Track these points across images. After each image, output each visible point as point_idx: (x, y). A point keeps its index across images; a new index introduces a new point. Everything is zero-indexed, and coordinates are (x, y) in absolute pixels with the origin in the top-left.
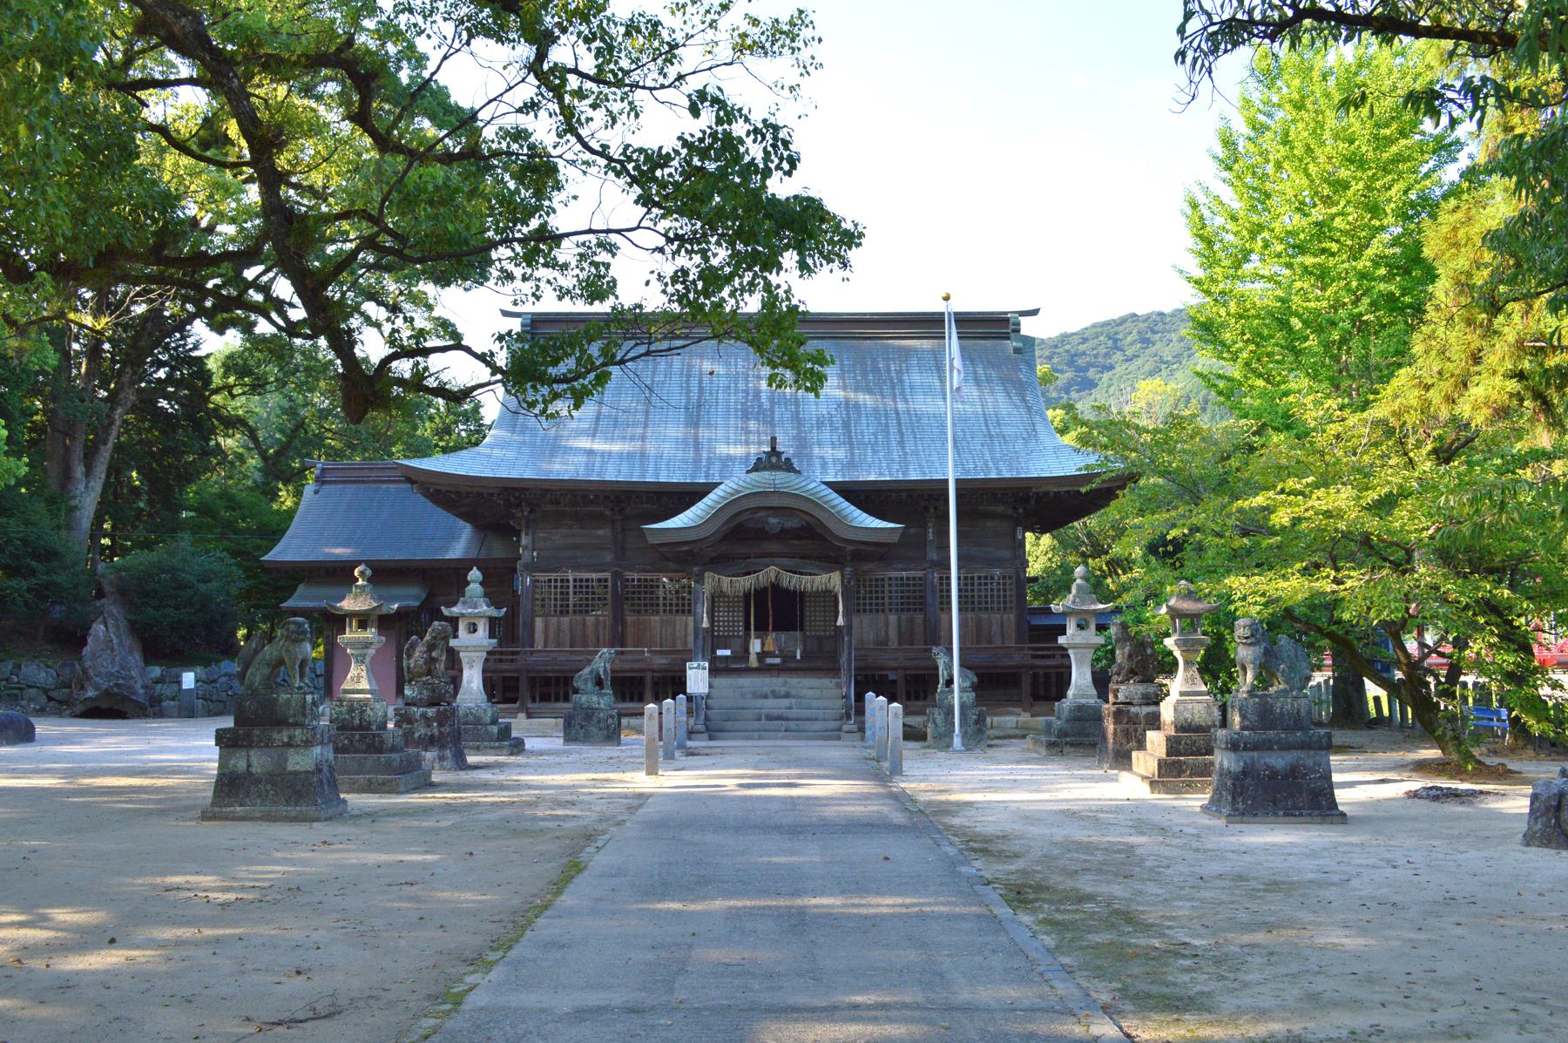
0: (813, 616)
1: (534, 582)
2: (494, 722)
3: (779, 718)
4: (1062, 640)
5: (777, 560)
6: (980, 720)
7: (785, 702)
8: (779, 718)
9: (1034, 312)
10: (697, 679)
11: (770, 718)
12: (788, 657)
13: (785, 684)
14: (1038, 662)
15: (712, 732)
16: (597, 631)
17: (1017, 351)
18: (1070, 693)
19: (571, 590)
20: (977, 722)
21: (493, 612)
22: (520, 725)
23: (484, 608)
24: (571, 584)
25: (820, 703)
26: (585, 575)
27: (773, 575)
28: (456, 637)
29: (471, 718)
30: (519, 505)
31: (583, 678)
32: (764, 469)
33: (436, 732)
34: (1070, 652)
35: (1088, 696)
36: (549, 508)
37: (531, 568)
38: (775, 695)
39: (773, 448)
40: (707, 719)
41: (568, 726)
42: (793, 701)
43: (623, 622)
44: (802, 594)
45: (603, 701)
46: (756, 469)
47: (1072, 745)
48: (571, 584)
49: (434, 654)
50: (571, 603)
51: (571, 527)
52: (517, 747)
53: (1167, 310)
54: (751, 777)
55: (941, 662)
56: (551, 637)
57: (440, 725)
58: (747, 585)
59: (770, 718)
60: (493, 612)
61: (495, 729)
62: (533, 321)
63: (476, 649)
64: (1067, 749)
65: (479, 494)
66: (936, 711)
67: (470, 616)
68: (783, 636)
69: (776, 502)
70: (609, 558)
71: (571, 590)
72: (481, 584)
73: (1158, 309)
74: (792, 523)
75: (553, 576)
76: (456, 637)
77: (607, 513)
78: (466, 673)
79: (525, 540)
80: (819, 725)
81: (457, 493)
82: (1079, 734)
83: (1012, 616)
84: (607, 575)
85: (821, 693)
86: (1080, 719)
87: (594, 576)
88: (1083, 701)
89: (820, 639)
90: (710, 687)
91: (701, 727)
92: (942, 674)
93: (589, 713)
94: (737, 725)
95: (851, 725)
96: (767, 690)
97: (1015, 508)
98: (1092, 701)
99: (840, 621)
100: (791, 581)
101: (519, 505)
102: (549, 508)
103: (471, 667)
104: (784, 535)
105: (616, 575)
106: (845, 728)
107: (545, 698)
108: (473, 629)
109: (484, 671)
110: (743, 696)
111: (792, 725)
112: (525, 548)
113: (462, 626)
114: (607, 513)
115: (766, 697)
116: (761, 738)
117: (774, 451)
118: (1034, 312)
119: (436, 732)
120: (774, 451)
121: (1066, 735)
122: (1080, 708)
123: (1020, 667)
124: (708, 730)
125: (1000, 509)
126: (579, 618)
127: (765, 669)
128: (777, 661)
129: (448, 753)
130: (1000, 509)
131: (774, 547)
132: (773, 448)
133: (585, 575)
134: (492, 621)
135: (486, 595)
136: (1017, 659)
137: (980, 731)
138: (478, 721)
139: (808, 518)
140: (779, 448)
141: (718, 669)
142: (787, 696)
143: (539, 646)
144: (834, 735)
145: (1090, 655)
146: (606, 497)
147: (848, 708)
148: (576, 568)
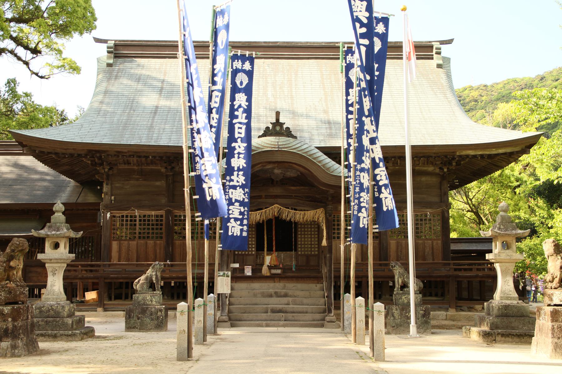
0: (304, 242)
1: (113, 217)
2: (71, 315)
3: (280, 311)
4: (488, 256)
5: (280, 200)
6: (426, 315)
7: (285, 300)
8: (280, 311)
9: (450, 42)
10: (223, 284)
11: (274, 311)
12: (286, 269)
13: (284, 288)
14: (461, 274)
15: (233, 321)
16: (155, 251)
17: (439, 66)
18: (497, 295)
19: (137, 223)
20: (424, 316)
21: (72, 234)
22: (92, 319)
23: (66, 231)
24: (138, 219)
25: (305, 301)
26: (148, 213)
27: (276, 210)
28: (43, 251)
29: (52, 312)
30: (102, 164)
31: (140, 282)
32: (271, 135)
33: (10, 326)
34: (497, 266)
35: (511, 298)
36: (122, 167)
37: (109, 208)
38: (277, 295)
39: (278, 120)
40: (230, 312)
41: (129, 317)
42: (290, 299)
43: (173, 245)
44: (296, 223)
45: (154, 300)
46: (264, 135)
47: (503, 335)
48: (138, 219)
49: (12, 264)
50: (137, 231)
51: (137, 180)
52: (89, 333)
53: (489, 84)
54: (333, 55)
55: (397, 271)
56: (123, 255)
57: (14, 320)
58: (258, 217)
59: (274, 311)
60: (72, 234)
61: (69, 321)
62: (116, 45)
63: (58, 261)
64: (499, 338)
65: (72, 155)
66: (394, 308)
67: (53, 236)
68: (282, 254)
69: (279, 159)
70: (164, 200)
71: (137, 223)
72: (64, 213)
73: (484, 83)
74: (291, 174)
75: (125, 213)
76: (43, 251)
77: (163, 170)
78: (50, 279)
79: (105, 189)
80: (309, 316)
81: (56, 154)
82: (507, 328)
83: (440, 242)
84: (162, 212)
85: (311, 294)
86: (506, 316)
87: (153, 213)
88: (508, 302)
89: (308, 257)
90: (232, 289)
91: (225, 318)
92: (398, 281)
93: (144, 310)
94: (251, 316)
95: (332, 316)
96: (272, 291)
97: (441, 169)
98: (515, 302)
99: (324, 243)
100: (288, 214)
101: (102, 164)
102: (122, 167)
103: (54, 274)
104: (285, 182)
105: (168, 213)
106: (328, 318)
107: (118, 297)
108: (56, 246)
109: (65, 278)
110: (255, 295)
111: (290, 316)
112: (106, 194)
113: (47, 245)
114: (163, 170)
115: (271, 296)
116: (267, 326)
117: (278, 123)
118: (450, 42)
119: (10, 326)
120: (278, 123)
121: (497, 328)
122: (506, 307)
123: (446, 276)
124: (230, 319)
125: (431, 169)
126: (142, 242)
127: (272, 277)
128: (279, 271)
129: (20, 343)
130: (431, 169)
131: (277, 191)
132: (278, 120)
133: (148, 213)
134: (71, 240)
135: (67, 222)
136: (443, 271)
137: (427, 322)
138: (57, 315)
139: (301, 169)
140: (281, 120)
141: (237, 277)
142: (286, 295)
143: (115, 261)
144: (320, 324)
145: (512, 268)
146: (161, 157)
147: (330, 304)
148: (140, 207)
